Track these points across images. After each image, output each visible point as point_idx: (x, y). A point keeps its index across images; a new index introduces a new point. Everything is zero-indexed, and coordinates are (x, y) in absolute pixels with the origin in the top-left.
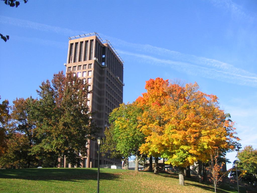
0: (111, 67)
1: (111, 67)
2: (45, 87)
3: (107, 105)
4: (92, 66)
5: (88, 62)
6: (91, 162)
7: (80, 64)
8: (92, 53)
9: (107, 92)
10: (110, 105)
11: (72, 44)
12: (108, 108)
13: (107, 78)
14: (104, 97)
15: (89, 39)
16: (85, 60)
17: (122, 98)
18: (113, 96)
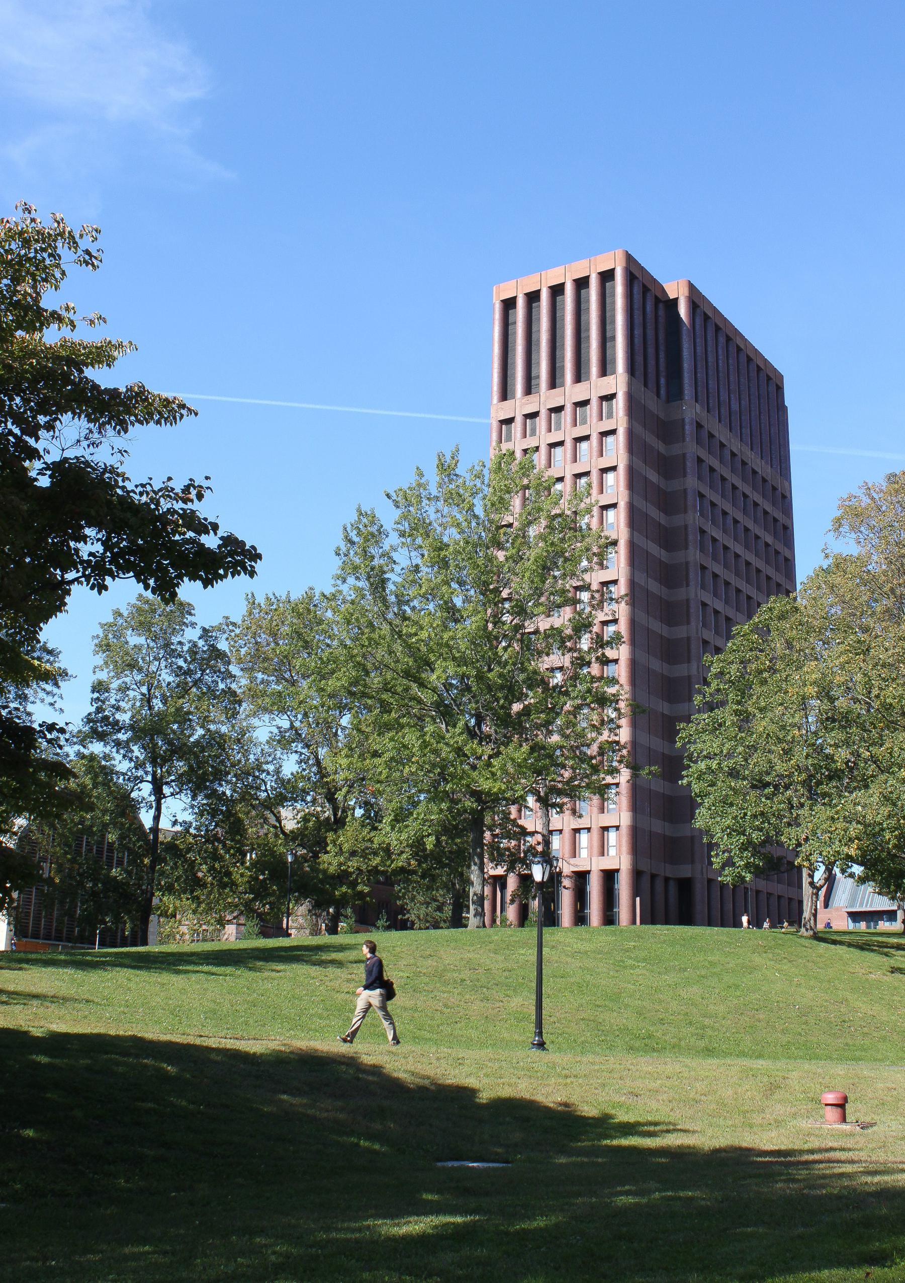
0: (713, 402)
1: (713, 402)
2: (365, 536)
3: (708, 598)
4: (620, 404)
5: (596, 386)
6: (638, 899)
7: (555, 398)
8: (613, 338)
9: (702, 532)
10: (775, 529)
11: (509, 304)
12: (716, 612)
13: (700, 461)
14: (691, 559)
15: (592, 268)
16: (553, 383)
17: (787, 553)
18: (739, 549)
